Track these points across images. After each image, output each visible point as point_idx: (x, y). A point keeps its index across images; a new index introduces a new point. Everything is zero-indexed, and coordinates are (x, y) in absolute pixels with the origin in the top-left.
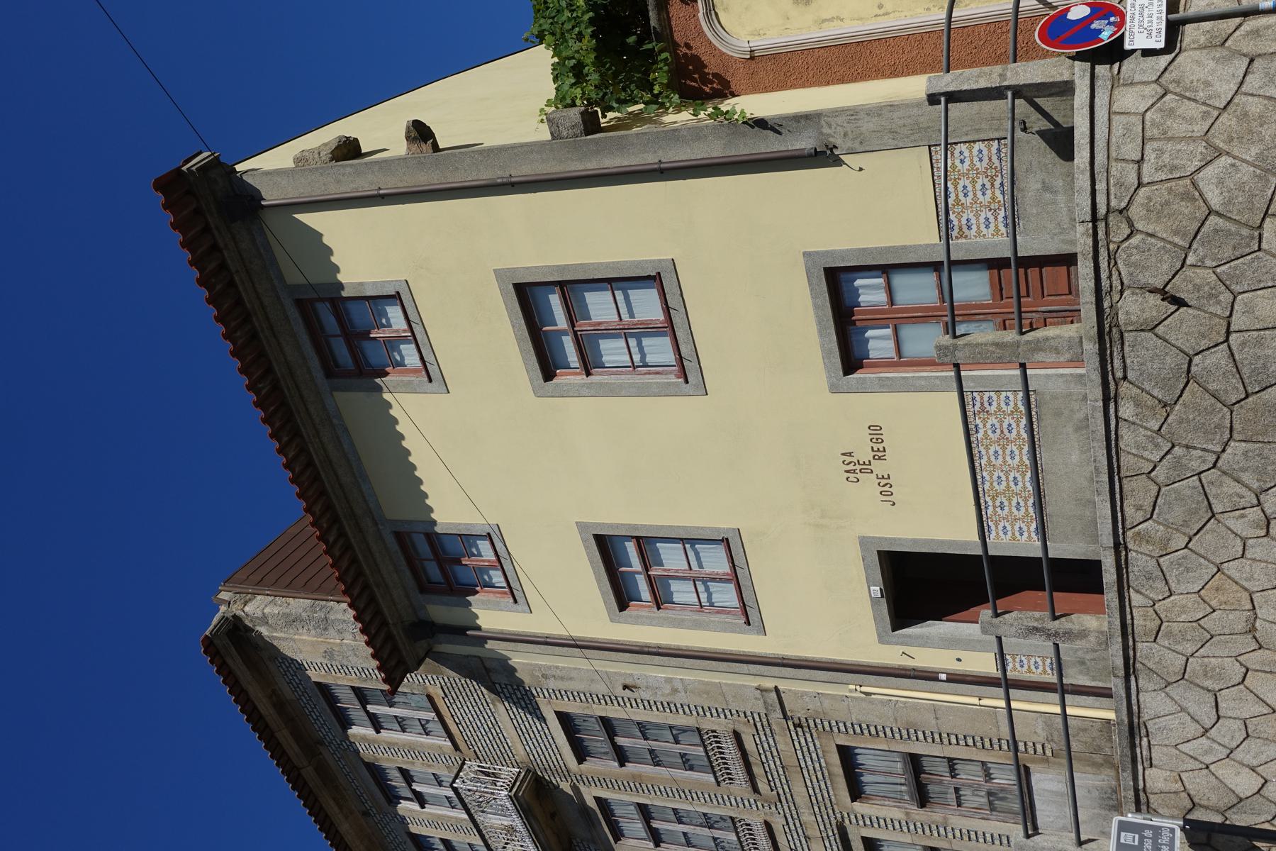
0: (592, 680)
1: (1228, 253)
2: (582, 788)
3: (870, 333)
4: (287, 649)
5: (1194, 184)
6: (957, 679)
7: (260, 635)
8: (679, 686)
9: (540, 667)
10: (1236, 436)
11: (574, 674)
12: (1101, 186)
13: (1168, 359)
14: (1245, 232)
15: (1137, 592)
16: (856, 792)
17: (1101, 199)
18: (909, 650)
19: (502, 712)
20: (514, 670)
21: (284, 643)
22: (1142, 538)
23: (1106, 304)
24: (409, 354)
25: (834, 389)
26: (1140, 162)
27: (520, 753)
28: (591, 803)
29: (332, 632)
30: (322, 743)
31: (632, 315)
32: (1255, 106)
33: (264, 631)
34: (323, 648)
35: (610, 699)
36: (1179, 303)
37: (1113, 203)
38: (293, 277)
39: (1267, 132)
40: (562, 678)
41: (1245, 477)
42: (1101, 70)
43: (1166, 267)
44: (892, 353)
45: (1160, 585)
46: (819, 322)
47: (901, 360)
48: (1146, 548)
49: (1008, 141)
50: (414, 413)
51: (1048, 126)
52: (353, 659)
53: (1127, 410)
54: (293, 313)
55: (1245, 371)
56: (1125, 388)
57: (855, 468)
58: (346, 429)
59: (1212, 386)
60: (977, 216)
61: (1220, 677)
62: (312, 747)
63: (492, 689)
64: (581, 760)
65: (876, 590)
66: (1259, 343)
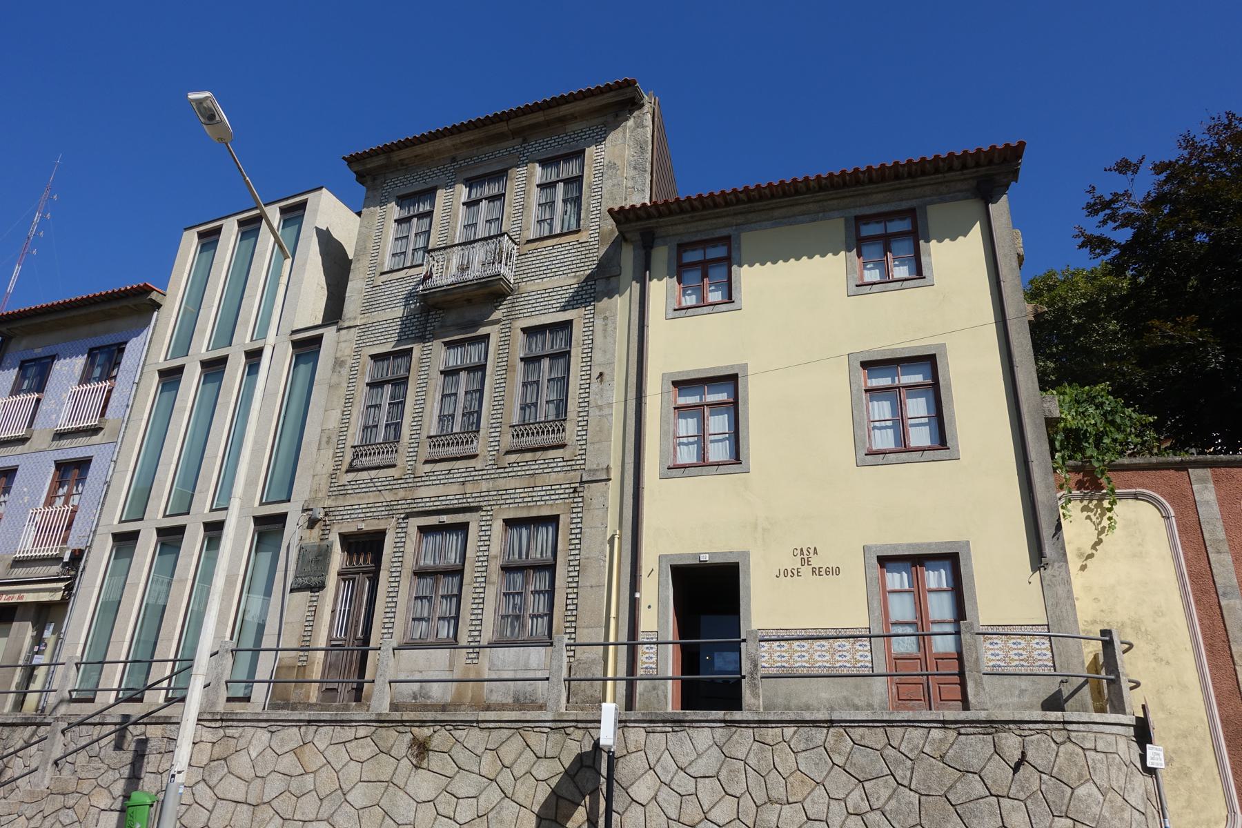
0: (605, 352)
1: (1050, 798)
2: (497, 327)
3: (905, 575)
4: (614, 137)
5: (1087, 781)
6: (634, 605)
7: (627, 120)
8: (606, 411)
9: (615, 315)
10: (923, 798)
11: (609, 339)
12: (1081, 727)
13: (975, 761)
14: (1064, 808)
15: (795, 732)
16: (510, 523)
17: (1074, 727)
18: (655, 574)
19: (569, 282)
20: (610, 297)
21: (620, 135)
22: (839, 738)
23: (1011, 726)
24: (690, 300)
25: (866, 549)
26: (1095, 750)
27: (530, 287)
28: (483, 331)
29: (632, 173)
30: (525, 141)
31: (712, 441)
32: (1127, 815)
33: (631, 123)
34: (619, 163)
35: (589, 361)
36: (1016, 769)
37: (1073, 734)
38: (935, 214)
39: (1116, 822)
40: (605, 330)
41: (893, 802)
42: (1131, 731)
43: (1039, 762)
44: (889, 588)
45: (803, 746)
46: (917, 545)
47: (885, 593)
48: (831, 740)
49: (1052, 672)
50: (828, 271)
51: (1065, 694)
52: (610, 183)
53: (936, 734)
54: (905, 205)
55: (972, 805)
56: (952, 734)
57: (805, 556)
58: (815, 221)
59: (959, 785)
60: (1000, 649)
61: (730, 780)
62: (524, 134)
63: (589, 278)
64: (524, 330)
65: (705, 558)
66: (992, 814)
